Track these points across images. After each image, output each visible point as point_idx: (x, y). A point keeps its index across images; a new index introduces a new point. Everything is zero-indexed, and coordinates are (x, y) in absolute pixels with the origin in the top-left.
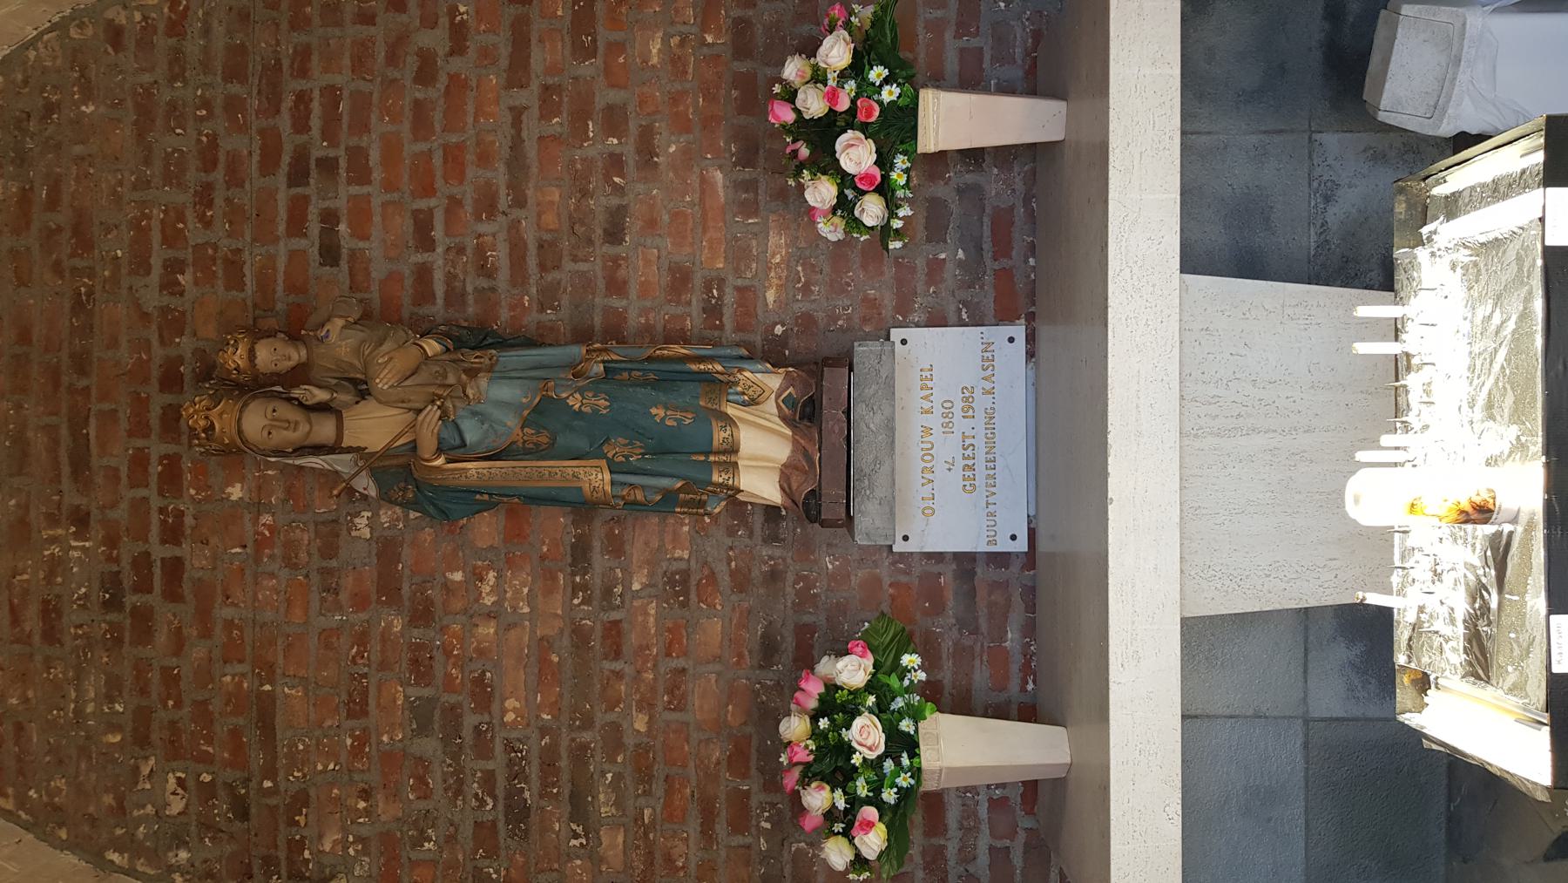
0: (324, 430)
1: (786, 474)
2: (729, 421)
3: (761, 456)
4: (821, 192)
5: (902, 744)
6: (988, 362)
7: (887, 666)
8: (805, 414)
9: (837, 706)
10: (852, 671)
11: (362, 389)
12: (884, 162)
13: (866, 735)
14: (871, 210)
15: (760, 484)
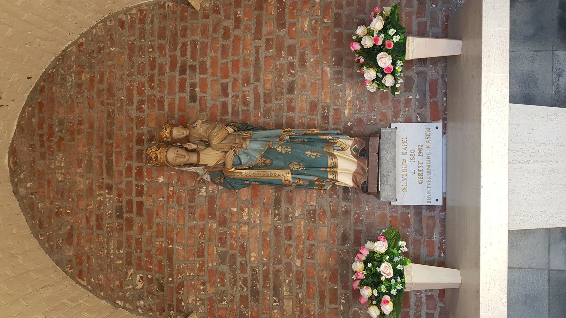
0: (193, 158)
1: (355, 177)
2: (334, 156)
4: (370, 74)
6: (428, 136)
7: (393, 245)
8: (362, 154)
9: (374, 259)
11: (208, 144)
14: (389, 81)
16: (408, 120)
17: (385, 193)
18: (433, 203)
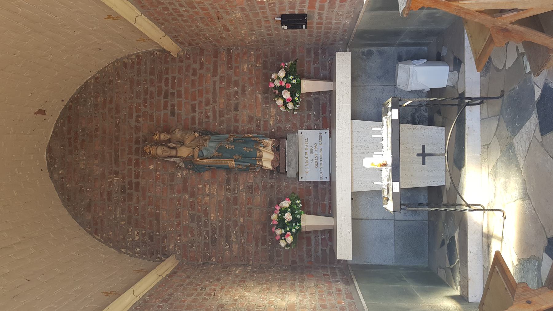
0: (173, 153)
1: (273, 162)
2: (260, 151)
3: (267, 159)
4: (280, 102)
5: (296, 220)
6: (320, 138)
7: (293, 203)
8: (277, 149)
9: (283, 211)
10: (286, 204)
11: (183, 144)
12: (293, 95)
13: (288, 217)
15: (267, 165)
16: (309, 128)
17: (291, 173)
18: (324, 180)
